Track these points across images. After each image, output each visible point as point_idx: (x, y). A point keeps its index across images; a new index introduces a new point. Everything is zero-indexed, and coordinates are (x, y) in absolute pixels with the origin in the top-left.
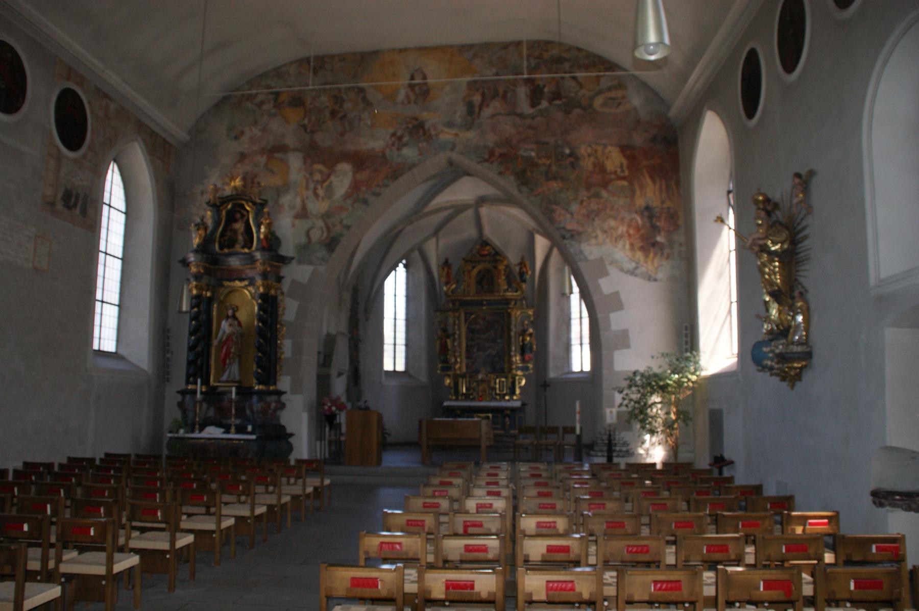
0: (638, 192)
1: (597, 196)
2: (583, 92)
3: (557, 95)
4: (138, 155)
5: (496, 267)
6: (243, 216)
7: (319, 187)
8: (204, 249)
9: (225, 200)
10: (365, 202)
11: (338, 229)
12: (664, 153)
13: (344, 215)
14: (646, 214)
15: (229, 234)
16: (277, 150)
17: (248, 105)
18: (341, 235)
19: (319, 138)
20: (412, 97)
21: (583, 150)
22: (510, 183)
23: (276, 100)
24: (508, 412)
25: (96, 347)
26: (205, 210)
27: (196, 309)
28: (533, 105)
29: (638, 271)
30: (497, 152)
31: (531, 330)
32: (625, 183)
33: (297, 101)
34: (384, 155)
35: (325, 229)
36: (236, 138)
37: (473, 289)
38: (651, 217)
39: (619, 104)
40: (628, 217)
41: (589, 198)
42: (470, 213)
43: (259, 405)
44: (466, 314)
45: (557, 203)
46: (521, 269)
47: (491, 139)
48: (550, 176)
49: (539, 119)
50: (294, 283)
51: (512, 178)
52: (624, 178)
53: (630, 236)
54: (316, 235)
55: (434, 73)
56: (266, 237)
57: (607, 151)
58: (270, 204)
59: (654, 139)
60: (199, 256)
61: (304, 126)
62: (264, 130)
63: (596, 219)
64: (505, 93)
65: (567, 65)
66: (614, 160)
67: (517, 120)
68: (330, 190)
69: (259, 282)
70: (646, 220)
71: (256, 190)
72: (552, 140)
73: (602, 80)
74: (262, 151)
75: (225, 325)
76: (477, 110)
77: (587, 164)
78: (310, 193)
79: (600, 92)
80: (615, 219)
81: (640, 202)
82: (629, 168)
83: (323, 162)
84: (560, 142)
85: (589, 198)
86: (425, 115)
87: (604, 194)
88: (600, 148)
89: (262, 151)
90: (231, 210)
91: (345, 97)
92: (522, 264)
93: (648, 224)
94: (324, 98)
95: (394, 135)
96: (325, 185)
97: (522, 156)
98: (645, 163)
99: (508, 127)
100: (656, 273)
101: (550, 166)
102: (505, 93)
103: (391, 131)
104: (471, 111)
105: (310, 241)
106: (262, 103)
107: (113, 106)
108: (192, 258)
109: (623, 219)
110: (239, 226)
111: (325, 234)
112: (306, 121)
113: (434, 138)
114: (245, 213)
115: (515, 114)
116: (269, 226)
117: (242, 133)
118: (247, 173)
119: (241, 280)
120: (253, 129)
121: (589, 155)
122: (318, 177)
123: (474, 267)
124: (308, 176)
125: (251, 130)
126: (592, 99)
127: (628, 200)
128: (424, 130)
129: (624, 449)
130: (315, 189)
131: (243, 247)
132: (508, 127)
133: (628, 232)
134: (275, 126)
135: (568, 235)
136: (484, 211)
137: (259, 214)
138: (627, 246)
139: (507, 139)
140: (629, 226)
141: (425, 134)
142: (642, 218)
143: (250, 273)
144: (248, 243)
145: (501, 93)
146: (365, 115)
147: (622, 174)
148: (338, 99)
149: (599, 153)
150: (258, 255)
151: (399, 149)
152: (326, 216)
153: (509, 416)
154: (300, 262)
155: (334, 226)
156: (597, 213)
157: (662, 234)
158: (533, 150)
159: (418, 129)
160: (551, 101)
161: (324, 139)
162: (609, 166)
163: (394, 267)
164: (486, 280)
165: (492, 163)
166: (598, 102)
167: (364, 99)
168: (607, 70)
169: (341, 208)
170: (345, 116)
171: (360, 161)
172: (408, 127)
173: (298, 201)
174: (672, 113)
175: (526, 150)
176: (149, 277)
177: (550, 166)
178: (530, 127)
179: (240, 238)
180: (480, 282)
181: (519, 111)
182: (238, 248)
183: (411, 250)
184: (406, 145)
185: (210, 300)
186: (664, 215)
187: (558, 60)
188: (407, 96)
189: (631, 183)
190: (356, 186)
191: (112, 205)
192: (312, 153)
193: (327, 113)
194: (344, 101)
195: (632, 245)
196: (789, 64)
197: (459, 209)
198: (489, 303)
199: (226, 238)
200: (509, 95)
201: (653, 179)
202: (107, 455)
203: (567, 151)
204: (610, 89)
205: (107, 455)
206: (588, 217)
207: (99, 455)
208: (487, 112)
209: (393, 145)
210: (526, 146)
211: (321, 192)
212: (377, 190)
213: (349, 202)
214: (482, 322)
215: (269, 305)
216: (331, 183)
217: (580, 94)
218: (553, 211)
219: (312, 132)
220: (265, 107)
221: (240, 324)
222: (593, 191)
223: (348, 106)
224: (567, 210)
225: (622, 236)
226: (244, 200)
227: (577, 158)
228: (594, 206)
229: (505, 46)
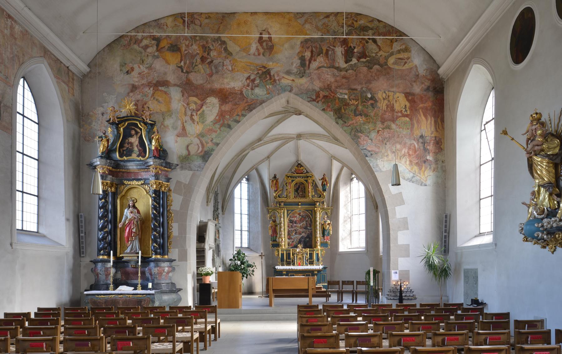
0: (416, 125)
1: (389, 127)
2: (381, 53)
3: (363, 55)
4: (44, 72)
5: (306, 181)
6: (137, 133)
7: (195, 114)
8: (107, 155)
9: (122, 120)
10: (229, 127)
11: (210, 145)
12: (437, 97)
13: (214, 135)
14: (421, 140)
15: (126, 145)
16: (160, 84)
17: (136, 47)
18: (213, 150)
19: (192, 76)
20: (262, 51)
21: (380, 95)
22: (328, 119)
23: (158, 45)
24: (316, 272)
25: (19, 226)
26: (107, 127)
27: (103, 201)
28: (346, 62)
29: (414, 179)
30: (322, 94)
31: (329, 222)
32: (407, 119)
33: (175, 48)
34: (242, 93)
35: (200, 145)
36: (128, 72)
37: (292, 195)
38: (424, 143)
39: (405, 63)
40: (408, 142)
41: (383, 129)
42: (291, 144)
43: (156, 269)
44: (288, 211)
45: (361, 132)
46: (323, 182)
47: (317, 85)
48: (357, 113)
49: (350, 71)
50: (178, 183)
51: (332, 113)
52: (407, 116)
53: (409, 155)
54: (193, 150)
55: (277, 33)
56: (156, 148)
57: (396, 96)
58: (158, 124)
59: (428, 89)
60: (104, 160)
61: (181, 67)
62: (150, 68)
63: (388, 143)
64: (327, 51)
65: (370, 32)
66: (401, 103)
67: (336, 71)
68: (202, 116)
69: (152, 180)
70: (421, 145)
71: (148, 113)
72: (359, 87)
73: (395, 44)
74: (149, 85)
75: (127, 212)
76: (307, 63)
77: (382, 105)
78: (188, 118)
79: (392, 54)
80: (400, 144)
81: (417, 133)
82: (411, 109)
83: (196, 96)
84: (364, 89)
85: (383, 129)
86: (270, 65)
87: (393, 126)
88: (391, 94)
89: (149, 85)
90: (127, 126)
91: (211, 47)
92: (323, 179)
93: (422, 148)
94: (195, 47)
95: (248, 78)
96: (199, 113)
97: (339, 98)
98: (421, 105)
99: (329, 76)
100: (426, 181)
101: (357, 105)
102: (327, 51)
103: (246, 75)
104: (304, 63)
105: (189, 154)
106: (146, 47)
107: (17, 28)
108: (97, 162)
109: (405, 144)
110: (134, 140)
111: (201, 149)
112: (182, 64)
113: (277, 81)
114: (139, 130)
115: (334, 67)
116: (158, 140)
117: (132, 69)
118: (138, 101)
119: (138, 180)
120: (141, 66)
121: (384, 99)
122: (193, 106)
123: (293, 181)
124: (185, 105)
125: (139, 67)
126: (387, 58)
127: (409, 131)
128: (270, 76)
129: (411, 295)
130: (192, 115)
131: (138, 156)
132: (329, 76)
133: (408, 153)
134: (159, 65)
135: (369, 154)
136: (302, 142)
137: (150, 133)
138: (408, 162)
139: (328, 85)
140: (409, 149)
141: (270, 79)
142: (418, 144)
143: (144, 175)
144: (143, 151)
145: (324, 52)
146: (227, 62)
147: (406, 113)
148: (206, 49)
149: (391, 98)
150: (151, 162)
151: (252, 89)
152: (201, 136)
153: (317, 275)
154: (182, 168)
155: (207, 143)
156: (389, 139)
157: (431, 154)
158: (346, 94)
159: (266, 74)
160: (359, 59)
161: (197, 78)
162: (397, 107)
163: (239, 181)
164: (301, 190)
165: (318, 102)
166: (391, 61)
167: (226, 49)
168: (400, 36)
169: (211, 131)
170: (212, 62)
171: (224, 96)
172: (258, 73)
173: (179, 123)
174: (440, 71)
175: (341, 94)
176: (63, 174)
177: (357, 105)
178: (344, 77)
179: (136, 149)
180: (296, 190)
181: (337, 65)
182: (134, 156)
183: (251, 169)
184: (257, 86)
185: (115, 195)
186: (432, 141)
187: (364, 29)
188: (257, 49)
189: (411, 119)
190: (222, 114)
191: (25, 115)
192: (188, 88)
193: (198, 59)
194: (211, 50)
195: (411, 161)
196: (223, 214)
197: (286, 139)
198: (303, 204)
199: (125, 149)
200: (330, 53)
201: (426, 116)
202: (39, 309)
203: (369, 96)
204: (399, 52)
205: (39, 309)
206: (382, 142)
207: (32, 311)
208: (314, 65)
209: (248, 86)
210: (341, 91)
211: (195, 118)
212: (238, 118)
213: (217, 126)
214: (298, 216)
215: (160, 198)
216: (203, 111)
217: (379, 55)
218: (359, 137)
219: (187, 72)
220: (149, 50)
221: (138, 212)
222: (386, 124)
223: (213, 54)
224: (368, 137)
225: (404, 155)
226: (137, 120)
227: (376, 101)
228: (386, 134)
229: (328, 15)
